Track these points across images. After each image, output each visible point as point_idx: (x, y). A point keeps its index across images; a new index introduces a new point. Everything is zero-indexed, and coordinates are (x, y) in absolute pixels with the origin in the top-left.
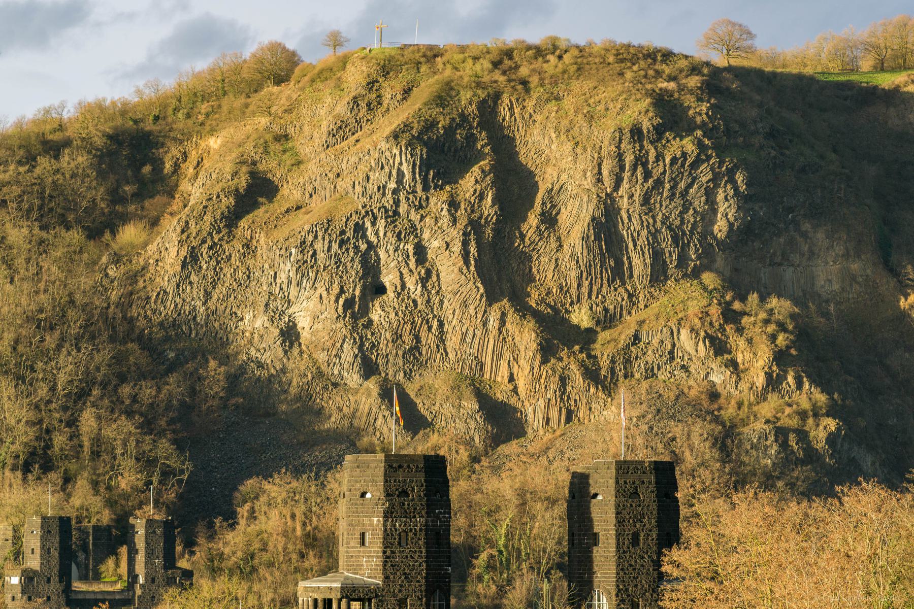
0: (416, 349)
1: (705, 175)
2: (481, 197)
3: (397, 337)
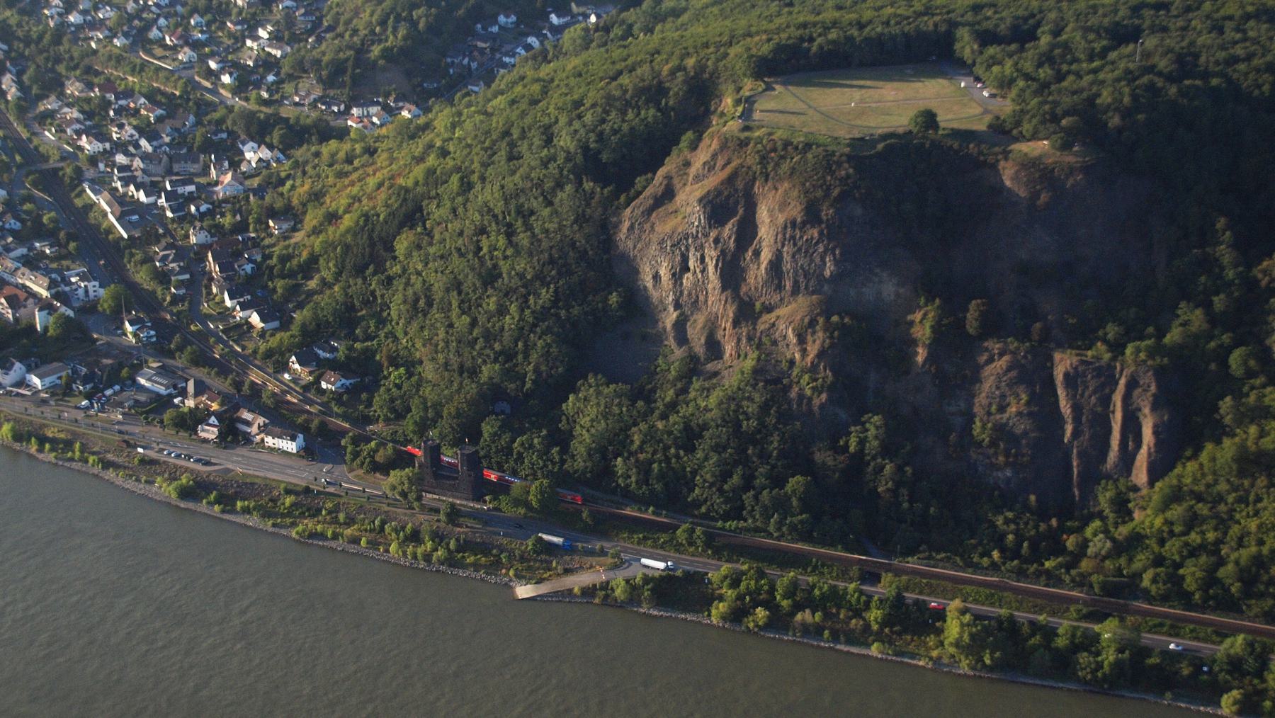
0: (697, 301)
1: (821, 248)
2: (730, 238)
3: (690, 294)
